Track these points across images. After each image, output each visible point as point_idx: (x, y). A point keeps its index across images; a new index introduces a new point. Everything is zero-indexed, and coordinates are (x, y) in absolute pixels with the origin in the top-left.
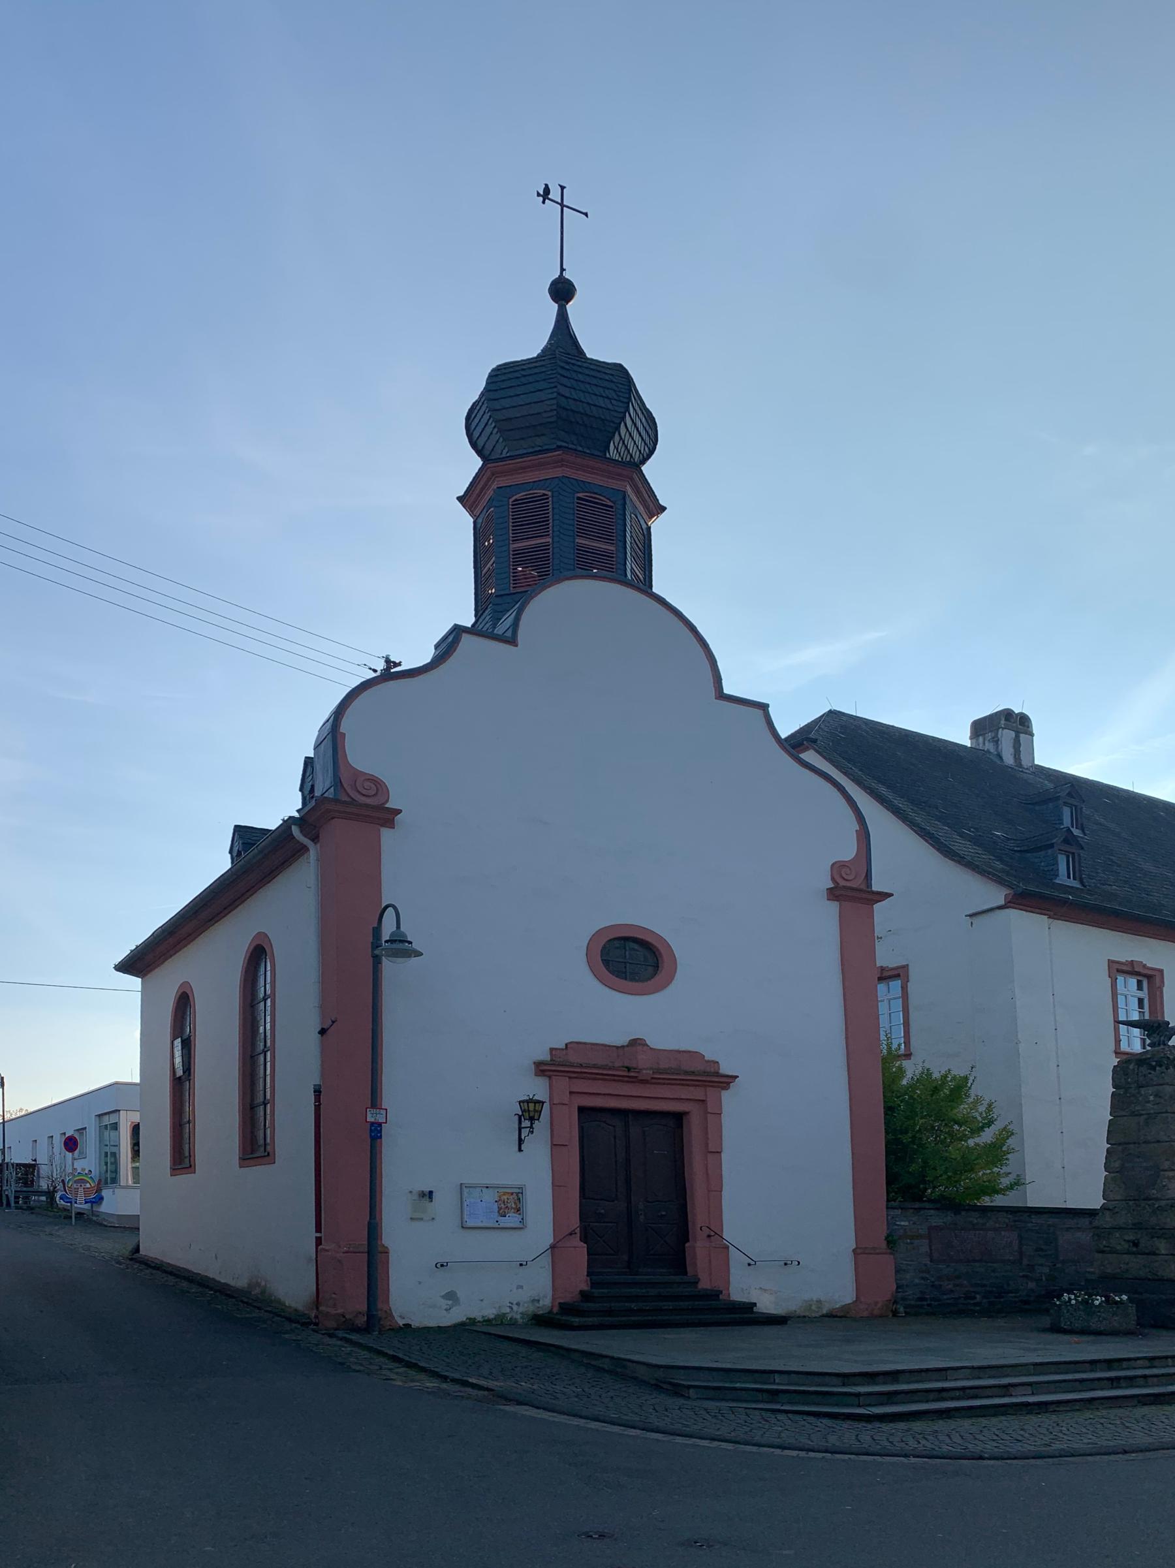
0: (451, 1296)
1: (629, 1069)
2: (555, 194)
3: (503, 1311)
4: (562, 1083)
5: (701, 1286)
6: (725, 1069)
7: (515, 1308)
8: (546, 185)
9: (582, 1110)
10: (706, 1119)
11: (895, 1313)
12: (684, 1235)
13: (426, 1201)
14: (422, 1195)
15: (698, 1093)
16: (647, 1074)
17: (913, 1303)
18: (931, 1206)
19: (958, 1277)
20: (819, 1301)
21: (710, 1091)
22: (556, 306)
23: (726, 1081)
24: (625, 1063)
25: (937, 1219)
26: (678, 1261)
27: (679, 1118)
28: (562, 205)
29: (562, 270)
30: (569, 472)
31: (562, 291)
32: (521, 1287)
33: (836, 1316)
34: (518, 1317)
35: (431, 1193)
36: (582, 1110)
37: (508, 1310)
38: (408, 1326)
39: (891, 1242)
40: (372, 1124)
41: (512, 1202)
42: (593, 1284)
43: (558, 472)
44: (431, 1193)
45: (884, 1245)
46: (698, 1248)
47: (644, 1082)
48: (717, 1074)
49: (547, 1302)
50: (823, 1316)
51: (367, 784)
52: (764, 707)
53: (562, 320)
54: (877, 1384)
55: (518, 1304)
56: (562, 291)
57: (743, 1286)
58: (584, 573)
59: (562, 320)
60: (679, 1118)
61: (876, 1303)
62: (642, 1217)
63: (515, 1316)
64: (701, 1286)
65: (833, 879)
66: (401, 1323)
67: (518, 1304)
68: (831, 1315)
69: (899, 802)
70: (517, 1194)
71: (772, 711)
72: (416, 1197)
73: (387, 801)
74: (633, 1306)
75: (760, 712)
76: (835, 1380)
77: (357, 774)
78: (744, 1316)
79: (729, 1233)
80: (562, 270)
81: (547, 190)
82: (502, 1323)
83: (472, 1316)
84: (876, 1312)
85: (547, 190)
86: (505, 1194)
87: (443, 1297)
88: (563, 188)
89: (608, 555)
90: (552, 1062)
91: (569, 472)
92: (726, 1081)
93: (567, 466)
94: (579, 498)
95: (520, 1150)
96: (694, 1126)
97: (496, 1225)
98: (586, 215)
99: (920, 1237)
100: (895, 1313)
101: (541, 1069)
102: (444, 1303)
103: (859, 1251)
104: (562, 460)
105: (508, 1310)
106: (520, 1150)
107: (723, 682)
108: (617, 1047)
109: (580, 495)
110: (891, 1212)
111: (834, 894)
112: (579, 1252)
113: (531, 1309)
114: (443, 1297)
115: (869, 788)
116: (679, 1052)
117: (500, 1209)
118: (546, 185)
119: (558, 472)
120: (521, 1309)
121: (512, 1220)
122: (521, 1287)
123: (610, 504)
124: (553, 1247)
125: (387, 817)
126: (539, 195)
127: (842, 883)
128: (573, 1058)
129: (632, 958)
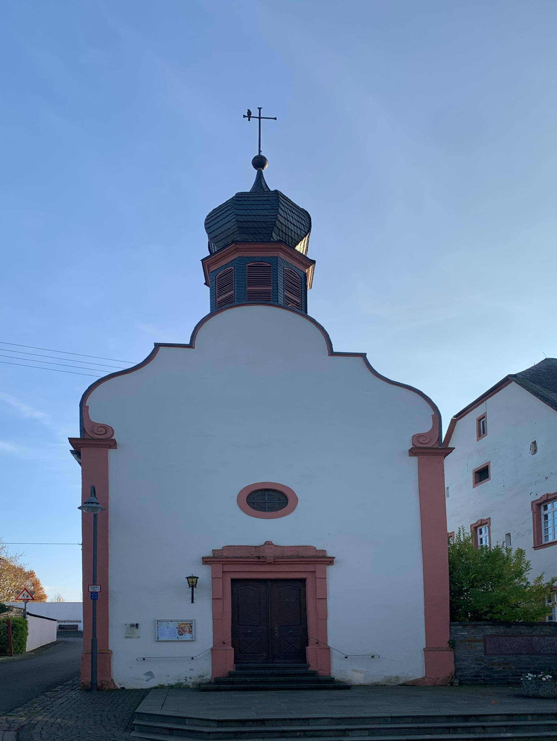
0: (150, 674)
1: (259, 558)
2: (255, 113)
3: (181, 681)
4: (219, 568)
5: (310, 669)
6: (329, 554)
7: (189, 680)
8: (249, 110)
9: (233, 581)
10: (316, 581)
11: (452, 684)
12: (306, 642)
13: (134, 629)
14: (132, 626)
15: (310, 568)
16: (270, 559)
17: (470, 678)
18: (486, 623)
19: (507, 664)
20: (397, 677)
21: (319, 567)
22: (256, 171)
23: (330, 561)
24: (257, 556)
25: (490, 630)
26: (302, 656)
27: (303, 581)
28: (260, 118)
29: (260, 151)
30: (241, 254)
31: (259, 162)
32: (192, 670)
33: (408, 685)
34: (191, 684)
35: (137, 625)
36: (233, 581)
37: (184, 681)
38: (123, 688)
39: (452, 645)
40: (92, 593)
41: (185, 629)
42: (237, 668)
43: (236, 256)
44: (137, 625)
45: (447, 645)
46: (311, 650)
47: (270, 564)
48: (325, 557)
49: (208, 677)
50: (400, 685)
51: (100, 429)
52: (363, 355)
53: (260, 176)
54: (470, 721)
55: (190, 678)
56: (259, 162)
57: (340, 670)
58: (231, 305)
59: (260, 176)
60: (303, 581)
61: (438, 679)
62: (277, 634)
63: (188, 684)
64: (310, 669)
65: (413, 444)
66: (119, 687)
67: (190, 678)
68: (404, 685)
69: (546, 393)
70: (190, 624)
71: (368, 357)
72: (129, 627)
73: (112, 435)
74: (248, 679)
75: (360, 359)
76: (410, 720)
77: (94, 424)
78: (345, 687)
79: (331, 643)
80: (260, 151)
81: (249, 113)
82: (180, 688)
83: (162, 684)
84: (437, 683)
85: (249, 113)
86: (182, 624)
87: (145, 674)
88: (260, 109)
89: (268, 292)
90: (214, 557)
91: (241, 254)
92: (330, 561)
93: (240, 251)
94: (249, 266)
95: (193, 602)
96: (309, 585)
97: (177, 639)
98: (275, 119)
99: (479, 641)
100: (452, 684)
101: (206, 561)
102: (145, 677)
103: (427, 649)
104: (236, 249)
105: (184, 681)
106: (193, 602)
107: (333, 346)
108: (256, 547)
109: (249, 265)
110: (453, 627)
111: (413, 452)
112: (230, 652)
113: (199, 680)
114: (145, 674)
115: (532, 390)
116: (299, 546)
117: (179, 631)
118: (249, 110)
119: (236, 256)
120: (192, 681)
121: (187, 636)
122: (192, 670)
123: (269, 265)
124: (212, 650)
125: (113, 444)
126: (244, 116)
127: (419, 445)
128: (225, 554)
129: (268, 500)
